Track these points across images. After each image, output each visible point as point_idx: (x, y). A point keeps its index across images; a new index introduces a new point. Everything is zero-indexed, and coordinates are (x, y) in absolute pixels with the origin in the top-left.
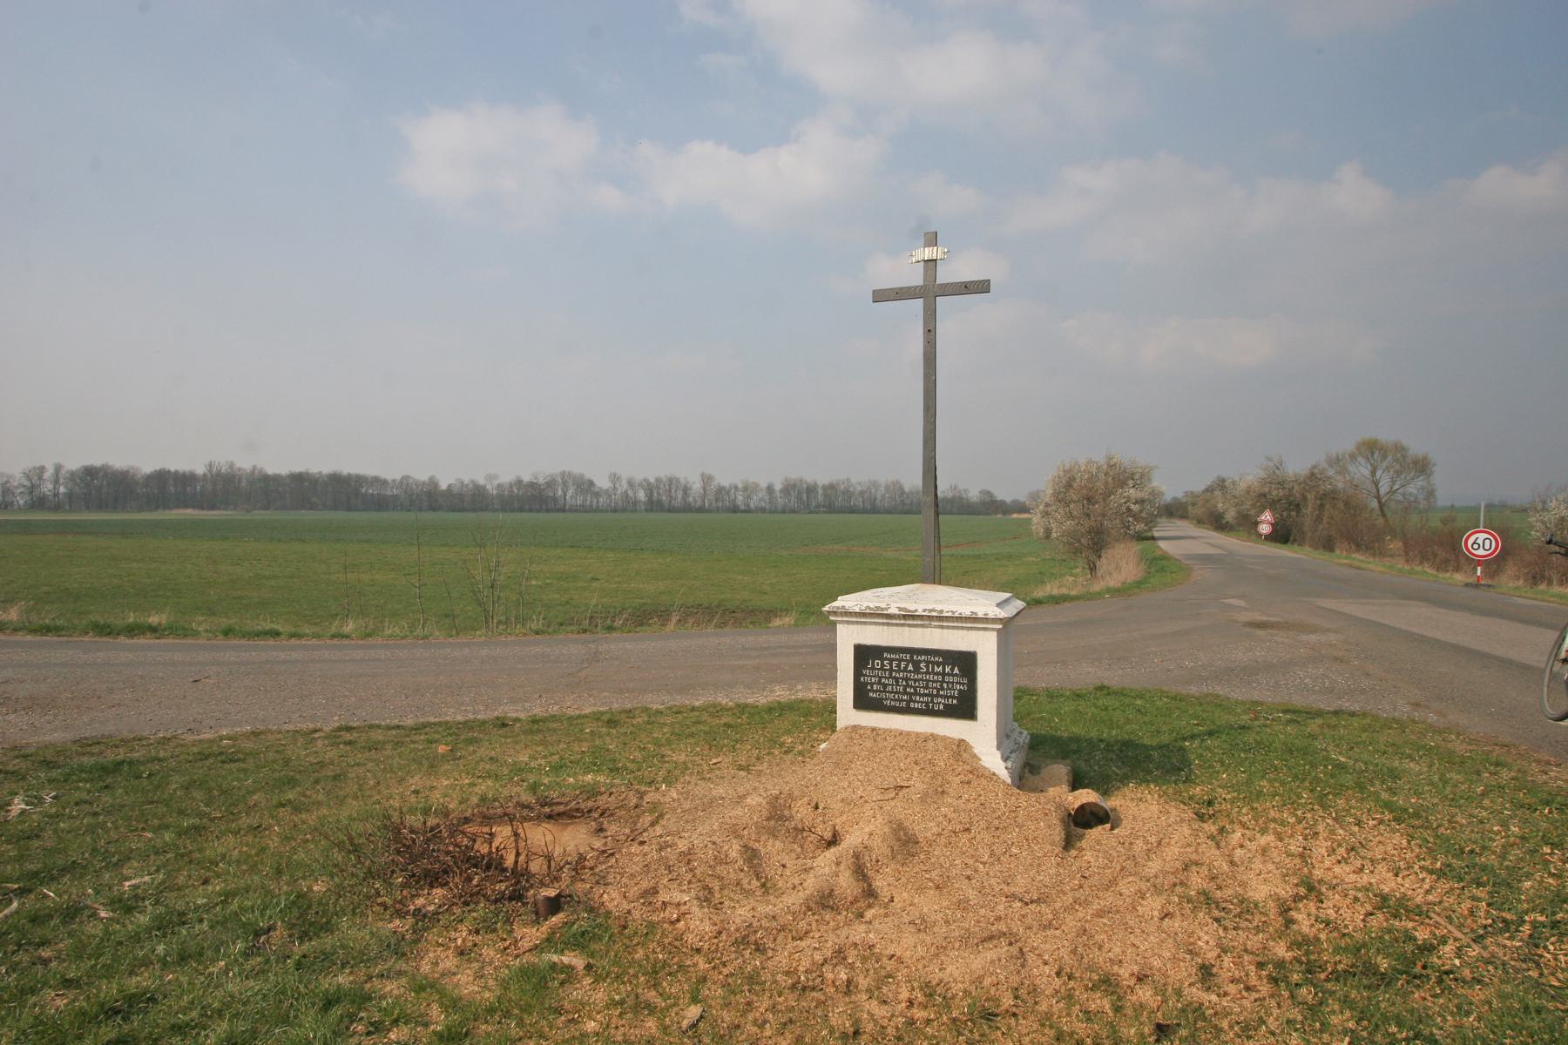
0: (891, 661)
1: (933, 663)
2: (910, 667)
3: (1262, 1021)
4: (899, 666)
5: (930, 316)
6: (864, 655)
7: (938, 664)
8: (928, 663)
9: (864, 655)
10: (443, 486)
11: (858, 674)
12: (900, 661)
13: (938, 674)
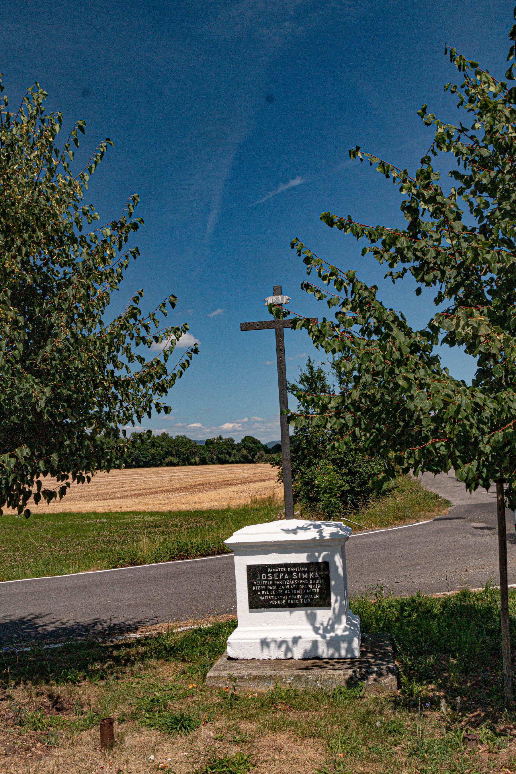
0: (273, 573)
1: (301, 572)
2: (286, 576)
3: (491, 686)
4: (278, 576)
5: (264, 326)
6: (253, 572)
7: (305, 572)
8: (298, 572)
9: (253, 572)
10: (475, 378)
11: (250, 585)
12: (279, 573)
13: (305, 579)
